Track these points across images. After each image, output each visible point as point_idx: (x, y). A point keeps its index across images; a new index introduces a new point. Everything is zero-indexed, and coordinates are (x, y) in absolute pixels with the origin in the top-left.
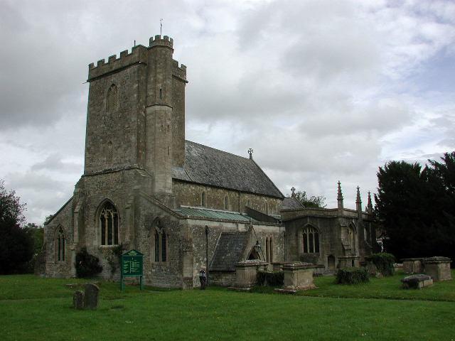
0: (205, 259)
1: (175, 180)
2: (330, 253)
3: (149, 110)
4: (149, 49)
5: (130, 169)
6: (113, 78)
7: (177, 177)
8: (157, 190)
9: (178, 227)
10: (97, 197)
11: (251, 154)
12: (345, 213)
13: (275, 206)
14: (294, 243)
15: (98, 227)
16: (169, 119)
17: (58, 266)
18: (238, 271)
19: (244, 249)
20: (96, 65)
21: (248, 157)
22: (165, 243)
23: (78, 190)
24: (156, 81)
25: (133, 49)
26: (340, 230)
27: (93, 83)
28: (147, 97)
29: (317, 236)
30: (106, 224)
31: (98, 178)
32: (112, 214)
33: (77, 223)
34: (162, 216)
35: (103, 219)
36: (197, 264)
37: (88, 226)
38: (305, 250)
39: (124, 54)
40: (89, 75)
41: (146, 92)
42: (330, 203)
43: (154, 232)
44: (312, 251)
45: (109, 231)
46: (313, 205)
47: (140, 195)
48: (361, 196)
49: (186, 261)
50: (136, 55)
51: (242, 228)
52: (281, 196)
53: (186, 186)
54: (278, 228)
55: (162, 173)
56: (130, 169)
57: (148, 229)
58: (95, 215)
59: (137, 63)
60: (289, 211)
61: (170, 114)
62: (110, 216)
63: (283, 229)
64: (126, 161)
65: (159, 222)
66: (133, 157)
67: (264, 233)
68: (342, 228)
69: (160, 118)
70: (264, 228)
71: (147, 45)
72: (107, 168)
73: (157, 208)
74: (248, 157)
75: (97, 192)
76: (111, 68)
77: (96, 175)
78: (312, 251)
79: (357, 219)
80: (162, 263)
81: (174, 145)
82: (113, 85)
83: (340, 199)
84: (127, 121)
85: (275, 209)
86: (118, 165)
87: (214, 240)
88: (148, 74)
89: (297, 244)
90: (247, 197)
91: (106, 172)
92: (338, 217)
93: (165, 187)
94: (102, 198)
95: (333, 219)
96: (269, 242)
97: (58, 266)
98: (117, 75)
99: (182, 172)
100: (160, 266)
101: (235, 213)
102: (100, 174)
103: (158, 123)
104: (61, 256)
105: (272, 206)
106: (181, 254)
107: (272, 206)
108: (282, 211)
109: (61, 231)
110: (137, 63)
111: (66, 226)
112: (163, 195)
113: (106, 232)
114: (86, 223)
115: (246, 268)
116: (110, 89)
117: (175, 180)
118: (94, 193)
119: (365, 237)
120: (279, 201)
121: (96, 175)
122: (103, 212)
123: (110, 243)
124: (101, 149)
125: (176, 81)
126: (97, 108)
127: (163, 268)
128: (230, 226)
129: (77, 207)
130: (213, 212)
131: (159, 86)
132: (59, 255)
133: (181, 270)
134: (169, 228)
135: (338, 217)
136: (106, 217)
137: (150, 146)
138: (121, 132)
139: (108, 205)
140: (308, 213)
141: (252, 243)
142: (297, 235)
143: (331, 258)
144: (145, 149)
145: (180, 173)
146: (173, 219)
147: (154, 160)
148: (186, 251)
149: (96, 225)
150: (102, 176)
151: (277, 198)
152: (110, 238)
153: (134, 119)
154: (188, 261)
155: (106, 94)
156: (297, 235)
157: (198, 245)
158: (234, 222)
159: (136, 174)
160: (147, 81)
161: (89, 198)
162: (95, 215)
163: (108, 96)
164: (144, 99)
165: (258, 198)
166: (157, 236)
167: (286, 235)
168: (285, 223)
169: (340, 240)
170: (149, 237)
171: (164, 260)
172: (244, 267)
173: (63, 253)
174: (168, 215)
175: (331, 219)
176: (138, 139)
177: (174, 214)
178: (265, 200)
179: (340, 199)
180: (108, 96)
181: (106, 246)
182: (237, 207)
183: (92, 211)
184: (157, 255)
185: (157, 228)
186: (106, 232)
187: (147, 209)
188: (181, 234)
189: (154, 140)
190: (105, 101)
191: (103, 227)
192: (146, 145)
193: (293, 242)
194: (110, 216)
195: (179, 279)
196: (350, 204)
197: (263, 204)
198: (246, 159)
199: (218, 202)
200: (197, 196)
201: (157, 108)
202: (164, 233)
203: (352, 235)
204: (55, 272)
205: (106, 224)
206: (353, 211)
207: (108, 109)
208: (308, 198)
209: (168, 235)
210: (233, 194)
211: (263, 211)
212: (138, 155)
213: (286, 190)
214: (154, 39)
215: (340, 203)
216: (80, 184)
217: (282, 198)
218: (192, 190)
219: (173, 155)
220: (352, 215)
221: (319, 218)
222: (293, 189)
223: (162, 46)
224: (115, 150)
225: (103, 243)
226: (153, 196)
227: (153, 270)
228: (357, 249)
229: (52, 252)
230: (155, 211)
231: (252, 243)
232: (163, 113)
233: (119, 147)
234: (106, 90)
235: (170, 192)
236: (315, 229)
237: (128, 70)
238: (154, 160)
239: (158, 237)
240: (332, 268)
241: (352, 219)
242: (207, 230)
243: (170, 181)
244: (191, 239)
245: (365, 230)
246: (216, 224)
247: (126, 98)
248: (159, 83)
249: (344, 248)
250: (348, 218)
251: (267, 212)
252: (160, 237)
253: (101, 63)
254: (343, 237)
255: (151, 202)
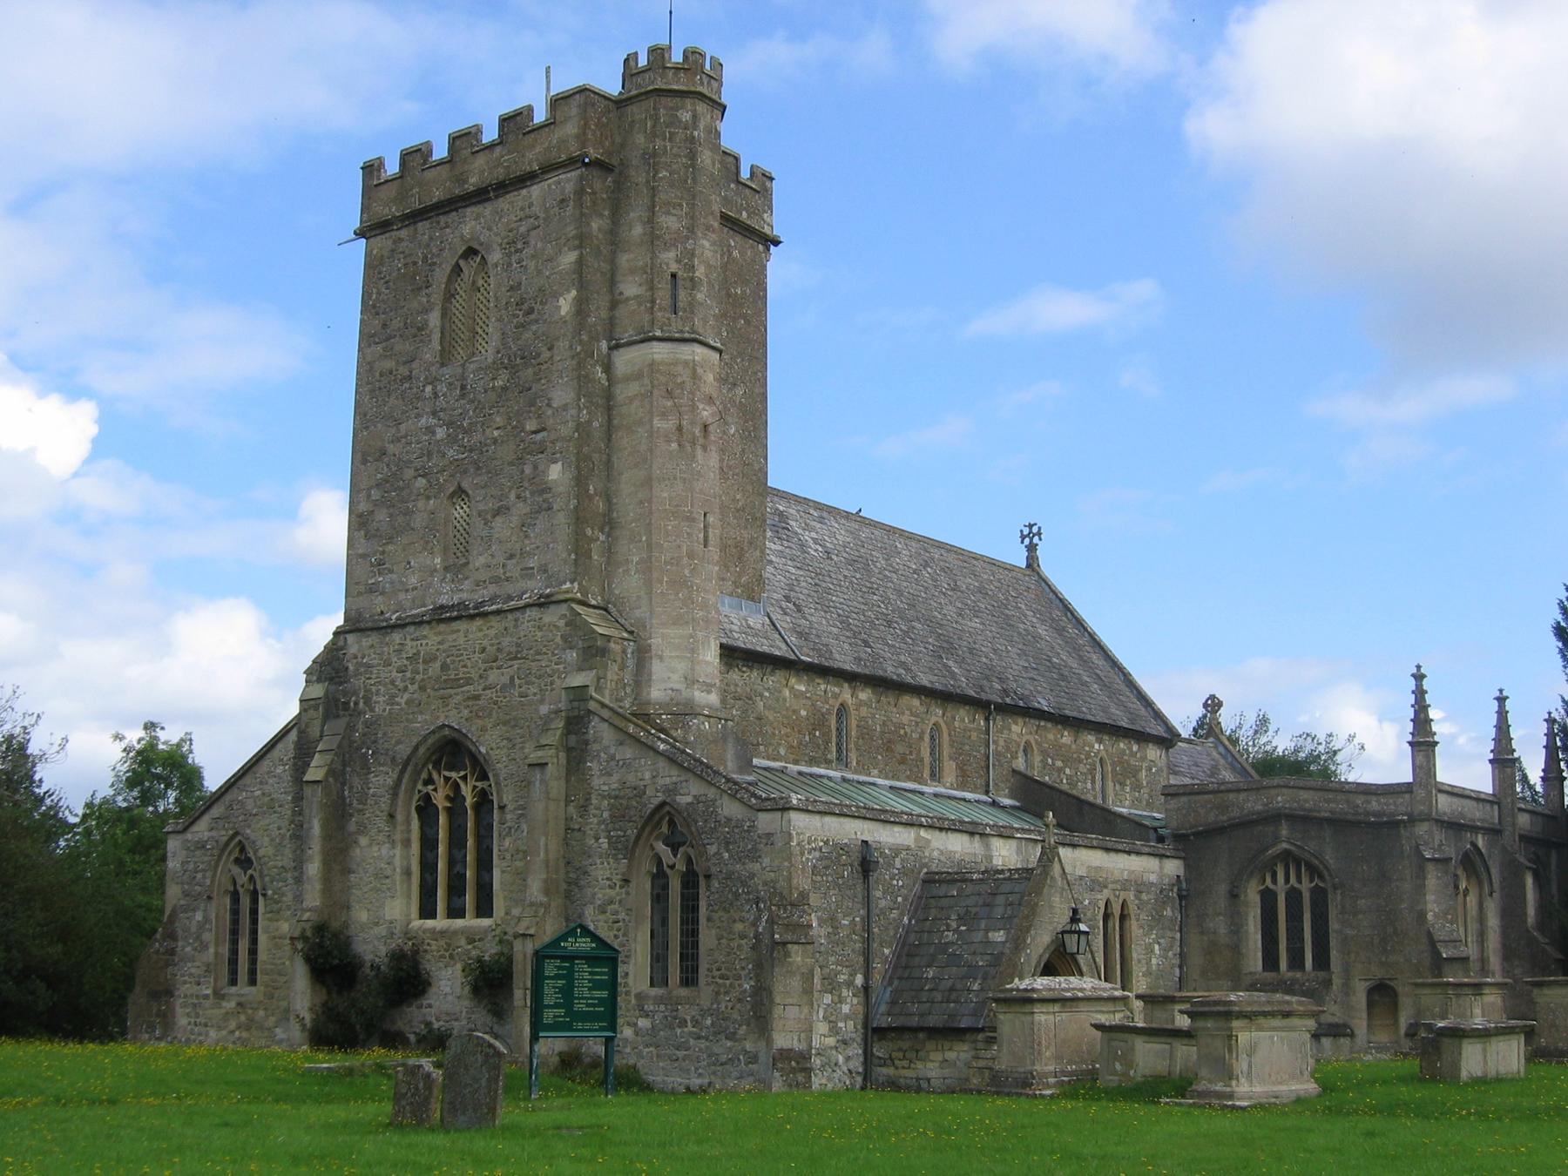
0: (859, 980)
1: (732, 655)
2: (1379, 973)
3: (625, 360)
4: (620, 103)
5: (544, 602)
6: (470, 225)
7: (741, 641)
8: (656, 693)
9: (751, 845)
10: (405, 715)
11: (1032, 548)
12: (1443, 803)
13: (1135, 772)
14: (1223, 930)
15: (407, 843)
16: (710, 400)
17: (230, 1005)
18: (1008, 1022)
19: (1018, 944)
20: (392, 167)
21: (1019, 559)
22: (695, 909)
23: (318, 691)
24: (653, 239)
25: (557, 102)
26: (1421, 874)
27: (383, 242)
28: (614, 305)
29: (1320, 900)
30: (442, 834)
31: (407, 641)
32: (466, 790)
33: (316, 828)
34: (684, 800)
35: (426, 810)
36: (828, 999)
37: (363, 841)
38: (1270, 961)
39: (515, 123)
40: (365, 208)
41: (612, 283)
42: (1374, 753)
43: (648, 866)
44: (1296, 961)
45: (452, 862)
46: (1306, 770)
47: (590, 712)
48: (1514, 733)
49: (786, 988)
50: (571, 129)
51: (1005, 854)
52: (1159, 730)
53: (774, 680)
54: (1153, 863)
55: (678, 621)
56: (544, 602)
57: (626, 849)
58: (395, 795)
59: (572, 162)
60: (1200, 791)
61: (710, 377)
62: (456, 797)
63: (1173, 867)
64: (527, 573)
65: (667, 822)
66: (560, 551)
67: (1096, 883)
68: (1430, 867)
69: (669, 394)
70: (1096, 858)
71: (611, 84)
72: (444, 600)
73: (662, 764)
74: (1019, 559)
75: (402, 700)
76: (461, 180)
77: (400, 626)
78: (1296, 961)
79: (1494, 832)
80: (684, 992)
81: (722, 507)
82: (471, 252)
83: (1423, 742)
84: (532, 404)
85: (1137, 787)
86: (493, 589)
87: (892, 898)
88: (617, 209)
89: (1237, 929)
90: (1018, 729)
91: (442, 616)
92: (1413, 820)
93: (691, 681)
94: (423, 723)
95: (1390, 826)
96: (1116, 919)
97: (230, 1005)
98: (487, 210)
99: (757, 621)
100: (671, 1002)
101: (968, 795)
102: (418, 623)
103: (664, 415)
104: (240, 965)
105: (1126, 773)
106: (767, 955)
107: (1126, 773)
108: (1170, 793)
109: (244, 862)
110: (572, 162)
111: (267, 837)
112: (685, 712)
113: (442, 865)
114: (352, 827)
115: (1037, 1008)
116: (457, 270)
117: (732, 655)
118: (391, 700)
119: (1531, 911)
120: (1153, 752)
121: (400, 626)
122: (429, 781)
123: (455, 912)
124: (419, 521)
125: (734, 241)
126: (400, 346)
127: (686, 1012)
128: (957, 846)
129: (317, 760)
130: (880, 787)
131: (669, 259)
132: (233, 962)
133: (760, 1016)
134: (712, 849)
135: (1413, 820)
136: (440, 800)
137: (627, 509)
138: (507, 452)
139: (452, 751)
140: (1281, 800)
141: (1054, 913)
142: (1234, 896)
143: (1383, 995)
144: (609, 523)
145: (748, 623)
146: (730, 809)
147: (646, 567)
148: (784, 944)
149: (398, 837)
150: (425, 630)
151: (1142, 737)
152: (456, 887)
153: (562, 394)
154: (796, 983)
155: (437, 292)
156: (1234, 896)
157: (832, 921)
158: (973, 830)
159: (574, 622)
160: (614, 238)
161: (367, 725)
162: (395, 795)
163: (449, 295)
164: (604, 314)
165: (1066, 738)
166: (660, 877)
167: (1186, 895)
168: (1184, 841)
169: (1422, 916)
170: (626, 881)
171: (690, 978)
172: (1031, 1001)
173: (253, 952)
174: (712, 793)
175: (1376, 827)
176: (580, 481)
177: (735, 790)
178: (1096, 745)
179: (1423, 742)
180: (449, 295)
181: (440, 922)
182: (975, 773)
183: (381, 780)
184: (659, 958)
185: (661, 847)
186: (442, 865)
187: (617, 769)
188: (763, 869)
189: (648, 482)
190: (434, 319)
191: (428, 844)
192: (610, 510)
193: (1220, 925)
194: (456, 797)
195: (753, 1058)
196: (1465, 767)
197: (1085, 767)
198: (1010, 568)
199: (900, 748)
200: (819, 721)
201: (660, 351)
202: (687, 858)
203: (1472, 900)
204: (213, 1034)
205: (442, 834)
206: (1477, 798)
207: (445, 357)
208: (1281, 743)
209: (708, 877)
210: (963, 717)
211: (1088, 790)
212: (580, 549)
213: (1182, 714)
214: (643, 61)
215: (1420, 758)
216: (329, 668)
217: (1168, 739)
218: (797, 695)
219: (724, 548)
220: (1476, 813)
221: (1330, 821)
222: (1213, 705)
223: (671, 89)
224: (478, 523)
225: (427, 911)
226: (643, 716)
227: (643, 1023)
228: (1495, 962)
229: (204, 947)
230: (654, 778)
231: (1054, 913)
232: (685, 376)
233: (497, 513)
234: (441, 275)
235: (714, 698)
236: (1314, 871)
237: (536, 191)
238: (646, 567)
239: (665, 887)
240: (1383, 1037)
241: (1474, 829)
242: (866, 862)
243: (711, 655)
244: (804, 896)
245: (1529, 881)
246: (901, 837)
247: (527, 307)
248: (667, 246)
249: (1437, 953)
250: (1454, 826)
251: (1104, 798)
252: (675, 885)
253: (415, 157)
254: (1433, 905)
255: (638, 740)
